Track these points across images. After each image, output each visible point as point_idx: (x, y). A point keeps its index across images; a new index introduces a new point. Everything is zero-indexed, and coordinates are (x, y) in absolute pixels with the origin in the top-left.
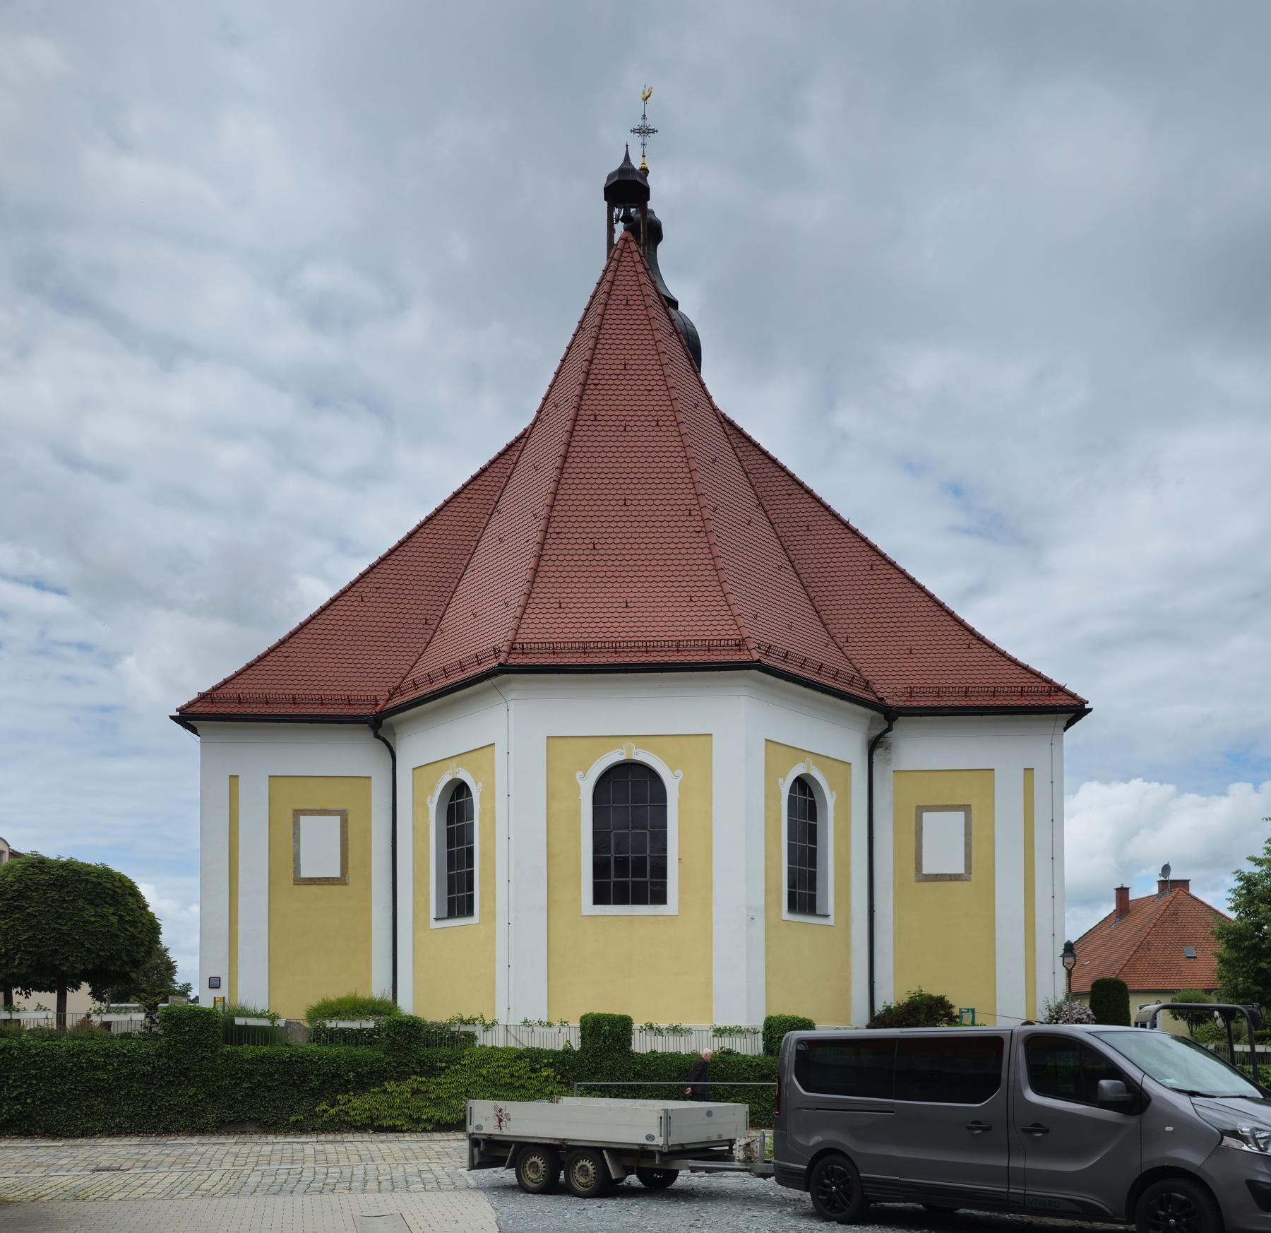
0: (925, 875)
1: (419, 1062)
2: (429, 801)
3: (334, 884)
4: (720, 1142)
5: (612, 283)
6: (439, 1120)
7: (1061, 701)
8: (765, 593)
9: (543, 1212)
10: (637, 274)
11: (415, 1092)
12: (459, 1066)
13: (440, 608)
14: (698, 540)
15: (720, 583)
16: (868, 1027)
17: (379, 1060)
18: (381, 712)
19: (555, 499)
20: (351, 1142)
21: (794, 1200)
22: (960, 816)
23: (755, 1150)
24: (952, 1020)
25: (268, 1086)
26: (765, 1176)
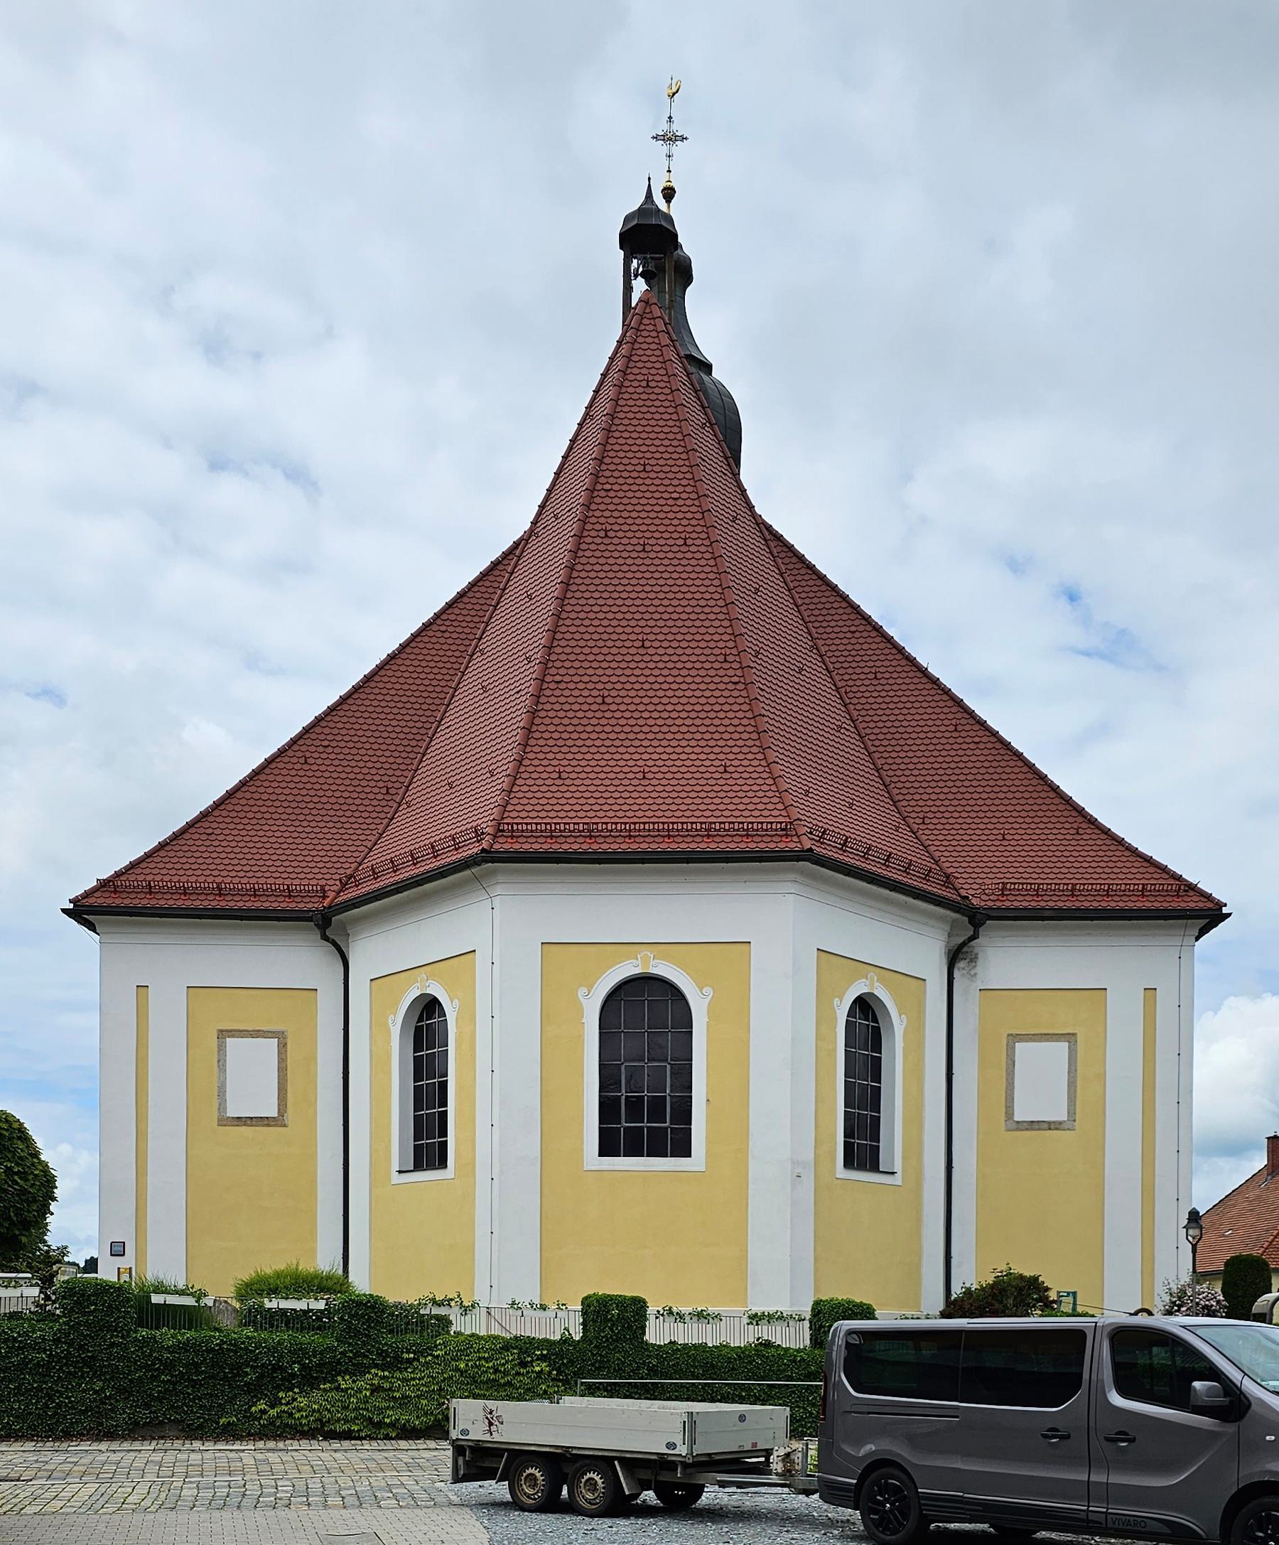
0: (1018, 1122)
1: (381, 1353)
2: (390, 1021)
3: (268, 1125)
4: (754, 1452)
5: (629, 358)
6: (404, 1425)
7: (1192, 903)
8: (819, 762)
9: (544, 1532)
10: (661, 347)
11: (376, 1390)
12: (430, 1358)
13: (405, 773)
14: (736, 693)
15: (763, 749)
16: (944, 1315)
17: (331, 1349)
18: (330, 907)
19: (554, 638)
20: (297, 1450)
21: (842, 1522)
22: (1063, 1046)
23: (796, 1461)
24: (1049, 1307)
25: (193, 1380)
26: (808, 1493)
